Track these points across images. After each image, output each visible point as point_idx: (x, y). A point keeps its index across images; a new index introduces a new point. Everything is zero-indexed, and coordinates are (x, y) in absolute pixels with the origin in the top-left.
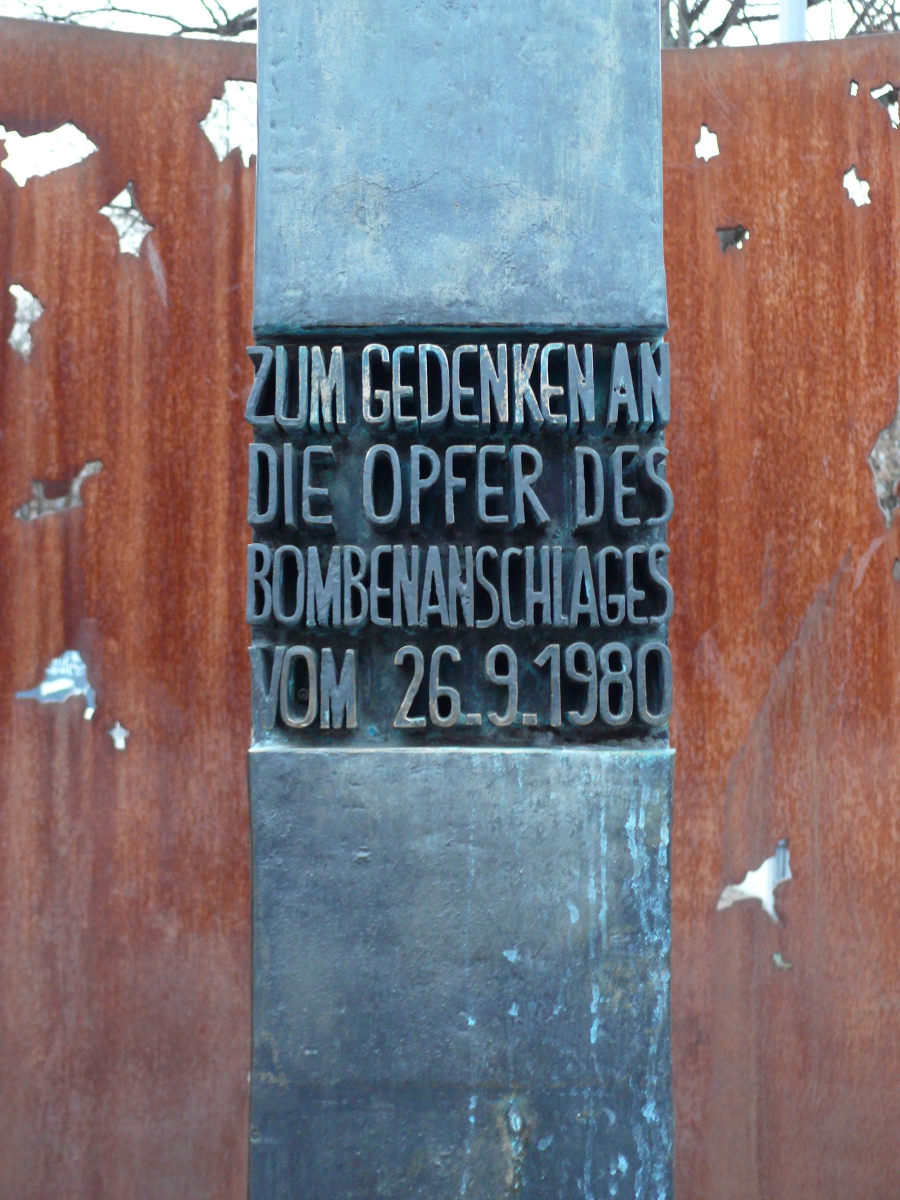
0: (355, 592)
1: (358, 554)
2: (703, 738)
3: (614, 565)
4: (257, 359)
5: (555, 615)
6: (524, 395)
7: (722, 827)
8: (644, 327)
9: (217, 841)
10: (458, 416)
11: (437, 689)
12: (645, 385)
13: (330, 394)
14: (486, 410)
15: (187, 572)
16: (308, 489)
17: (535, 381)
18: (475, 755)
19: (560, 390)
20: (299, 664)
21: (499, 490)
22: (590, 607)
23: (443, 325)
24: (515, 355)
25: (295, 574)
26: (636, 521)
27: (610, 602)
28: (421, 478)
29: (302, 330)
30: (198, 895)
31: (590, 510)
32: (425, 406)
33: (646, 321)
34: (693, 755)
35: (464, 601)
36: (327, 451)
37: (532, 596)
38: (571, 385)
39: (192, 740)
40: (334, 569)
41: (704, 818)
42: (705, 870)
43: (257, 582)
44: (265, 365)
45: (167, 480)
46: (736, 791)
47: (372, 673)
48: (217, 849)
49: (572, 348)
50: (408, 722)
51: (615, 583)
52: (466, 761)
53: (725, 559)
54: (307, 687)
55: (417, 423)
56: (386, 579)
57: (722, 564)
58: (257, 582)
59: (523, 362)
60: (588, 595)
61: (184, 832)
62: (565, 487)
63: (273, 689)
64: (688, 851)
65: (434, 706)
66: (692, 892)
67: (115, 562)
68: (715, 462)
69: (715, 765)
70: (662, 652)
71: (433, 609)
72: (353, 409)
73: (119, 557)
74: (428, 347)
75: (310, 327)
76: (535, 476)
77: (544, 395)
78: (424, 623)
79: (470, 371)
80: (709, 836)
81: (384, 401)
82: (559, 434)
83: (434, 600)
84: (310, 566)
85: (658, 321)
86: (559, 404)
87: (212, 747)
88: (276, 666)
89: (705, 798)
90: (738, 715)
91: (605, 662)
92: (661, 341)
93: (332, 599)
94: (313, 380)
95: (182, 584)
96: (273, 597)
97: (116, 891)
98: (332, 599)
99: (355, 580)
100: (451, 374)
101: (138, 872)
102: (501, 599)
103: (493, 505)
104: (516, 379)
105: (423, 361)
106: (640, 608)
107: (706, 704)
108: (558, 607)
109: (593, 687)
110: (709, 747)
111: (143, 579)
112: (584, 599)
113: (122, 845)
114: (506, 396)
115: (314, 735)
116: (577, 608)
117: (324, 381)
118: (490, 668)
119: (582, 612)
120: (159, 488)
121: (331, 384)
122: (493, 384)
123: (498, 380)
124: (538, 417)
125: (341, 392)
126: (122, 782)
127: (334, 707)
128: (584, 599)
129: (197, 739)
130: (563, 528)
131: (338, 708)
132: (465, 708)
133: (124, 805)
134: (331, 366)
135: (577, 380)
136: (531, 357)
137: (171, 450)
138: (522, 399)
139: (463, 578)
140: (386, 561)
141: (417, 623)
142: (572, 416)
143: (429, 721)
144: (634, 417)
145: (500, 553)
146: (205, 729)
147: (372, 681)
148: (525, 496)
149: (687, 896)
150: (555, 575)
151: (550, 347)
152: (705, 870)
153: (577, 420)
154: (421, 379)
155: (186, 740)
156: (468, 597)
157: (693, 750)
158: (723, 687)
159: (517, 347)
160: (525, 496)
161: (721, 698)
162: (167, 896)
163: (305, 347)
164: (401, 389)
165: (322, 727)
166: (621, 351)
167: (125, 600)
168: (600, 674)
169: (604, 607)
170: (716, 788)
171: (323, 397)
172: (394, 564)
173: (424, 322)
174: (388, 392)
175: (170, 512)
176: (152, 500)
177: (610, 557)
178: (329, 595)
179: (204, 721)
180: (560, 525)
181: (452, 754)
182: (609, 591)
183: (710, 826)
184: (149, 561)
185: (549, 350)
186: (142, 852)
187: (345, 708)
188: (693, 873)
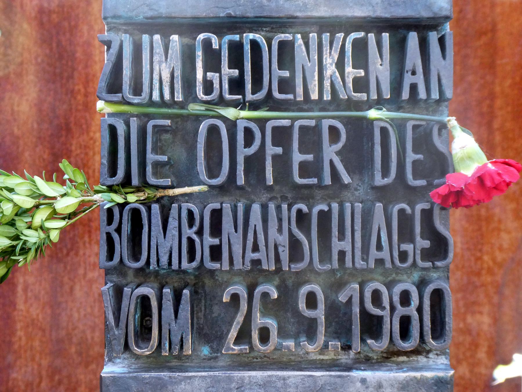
0: (191, 241)
1: (192, 209)
2: (480, 250)
3: (405, 221)
4: (109, 44)
5: (356, 260)
6: (331, 76)
7: (496, 320)
8: (433, 18)
9: (97, 334)
10: (276, 95)
11: (259, 320)
12: (432, 68)
13: (169, 76)
14: (300, 90)
15: (72, 119)
16: (151, 157)
17: (340, 65)
18: (289, 377)
19: (362, 73)
20: (145, 300)
21: (310, 157)
22: (385, 254)
23: (264, 17)
24: (324, 42)
25: (141, 227)
26: (421, 183)
27: (401, 250)
28: (245, 148)
29: (146, 20)
30: (82, 377)
31: (385, 173)
32: (249, 86)
33: (434, 13)
34: (473, 264)
35: (280, 249)
36: (167, 124)
37: (337, 245)
38: (371, 68)
39: (77, 254)
40: (173, 223)
41: (481, 313)
42: (482, 354)
43: (109, 235)
44: (114, 50)
45: (54, 45)
46: (507, 292)
47: (206, 302)
48: (97, 339)
49: (372, 36)
50: (234, 350)
51: (406, 233)
52: (282, 382)
53: (501, 109)
54: (151, 316)
55: (242, 101)
56: (216, 229)
57: (499, 113)
58: (109, 235)
59: (331, 48)
60: (383, 244)
61: (70, 327)
62: (365, 147)
63: (122, 324)
64: (468, 339)
65: (255, 336)
66: (471, 372)
67: (13, 112)
68: (494, 30)
69: (490, 271)
70: (444, 291)
71: (256, 256)
72: (189, 84)
73: (16, 108)
74: (251, 36)
75: (151, 18)
76: (340, 145)
77: (348, 77)
78: (248, 266)
79: (286, 51)
80: (485, 328)
81: (214, 81)
82: (360, 104)
83: (256, 248)
84: (153, 221)
85: (444, 13)
86: (361, 85)
87: (92, 259)
88: (125, 302)
89: (482, 297)
90: (509, 232)
91: (396, 299)
92: (447, 28)
93: (171, 248)
94: (154, 64)
95: (68, 130)
96: (122, 247)
97: (14, 375)
98: (171, 248)
99: (189, 232)
100: (270, 59)
101: (33, 360)
102: (310, 245)
103: (305, 169)
104: (324, 63)
105: (247, 48)
106: (427, 255)
107: (484, 223)
108: (358, 253)
109: (387, 320)
110: (486, 258)
111: (35, 126)
112: (379, 247)
113: (20, 339)
114: (316, 78)
115: (157, 362)
116: (374, 253)
117: (164, 65)
118: (302, 305)
119: (378, 257)
120: (48, 51)
121: (169, 68)
122: (306, 68)
123: (309, 65)
124: (343, 96)
125: (178, 73)
126: (20, 289)
127: (173, 338)
128: (379, 247)
129: (81, 252)
130: (363, 182)
131: (176, 340)
132: (282, 333)
133: (21, 306)
134: (170, 51)
135: (375, 64)
136: (337, 45)
137: (56, 20)
138: (329, 80)
139: (280, 230)
140: (217, 215)
141: (241, 267)
142: (371, 94)
143: (252, 348)
144: (422, 94)
145: (310, 209)
146: (87, 245)
147: (205, 309)
148: (331, 162)
149: (468, 375)
150: (356, 228)
151: (354, 35)
152: (482, 354)
153: (376, 97)
154: (246, 63)
155: (72, 253)
156: (284, 246)
157: (473, 259)
158: (497, 210)
159: (326, 36)
160: (331, 162)
161: (496, 219)
162: (57, 378)
163: (147, 36)
164: (228, 72)
165: (164, 354)
166: (413, 38)
167: (21, 142)
168: (393, 309)
169: (396, 254)
170: (491, 290)
171: (163, 78)
172: (223, 218)
173: (249, 15)
174: (218, 75)
175: (58, 71)
176: (43, 61)
177: (402, 212)
178: (169, 245)
179: (86, 239)
180: (361, 180)
181: (269, 376)
182: (402, 239)
183: (486, 320)
184: (40, 111)
185: (353, 38)
186: (36, 344)
187: (182, 338)
188: (472, 356)
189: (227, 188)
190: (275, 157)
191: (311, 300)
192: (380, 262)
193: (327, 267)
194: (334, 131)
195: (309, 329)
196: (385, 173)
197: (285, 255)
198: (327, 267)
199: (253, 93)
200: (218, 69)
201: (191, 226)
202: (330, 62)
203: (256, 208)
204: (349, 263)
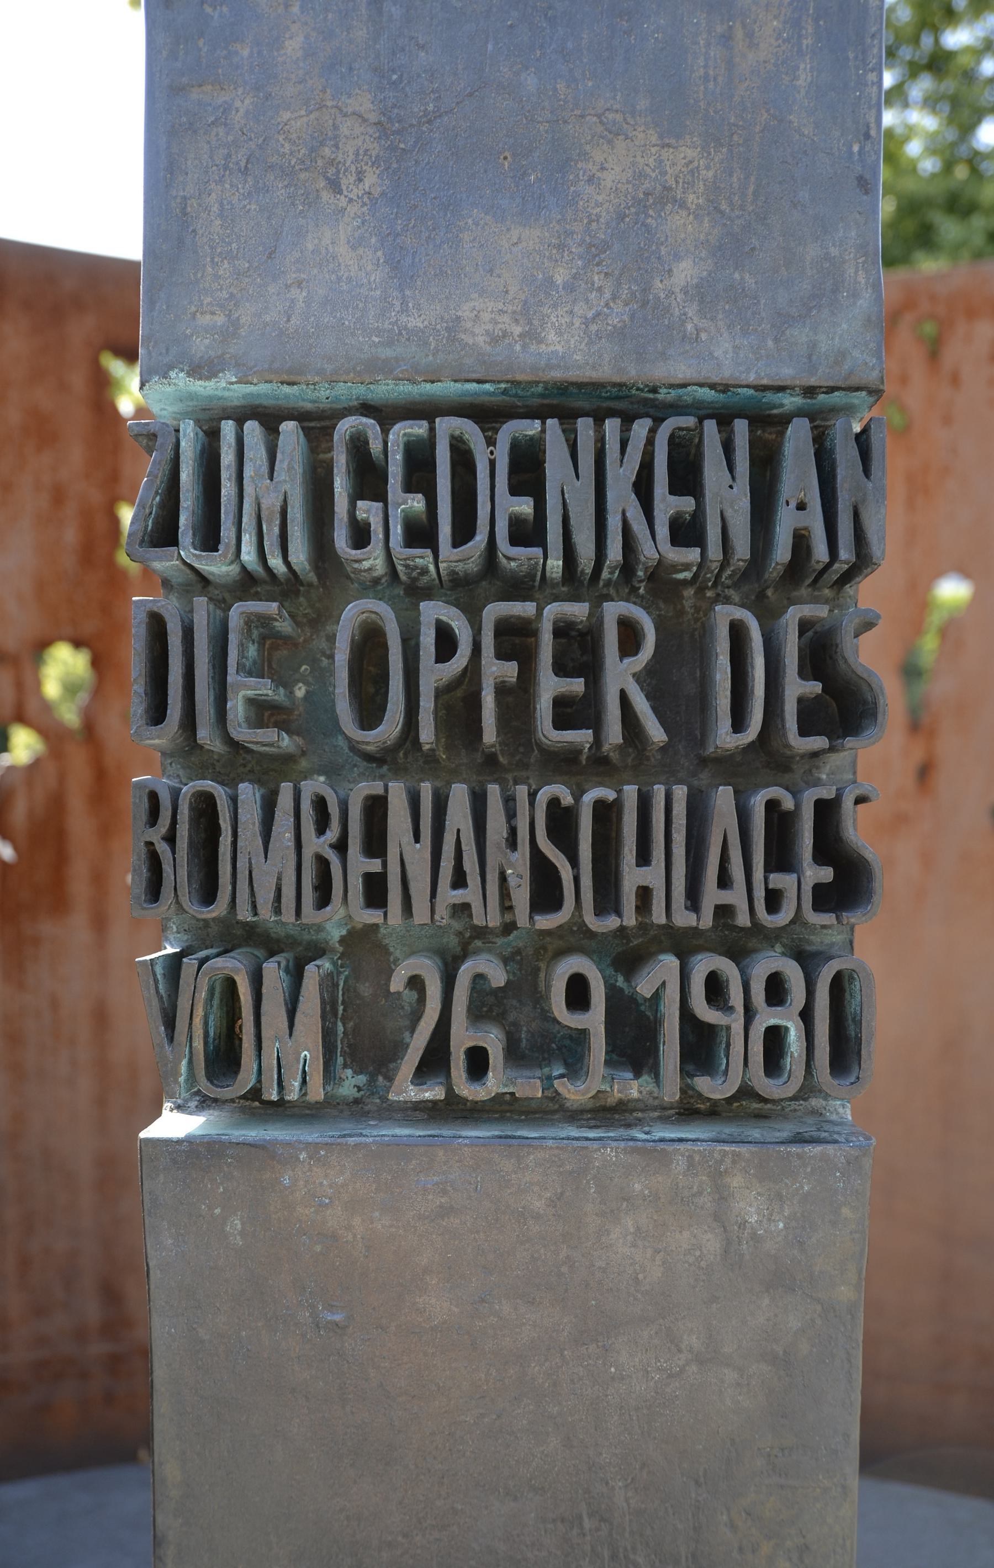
0: (323, 864)
3: (780, 823)
27: (771, 886)
31: (738, 724)
37: (632, 877)
51: (781, 856)
56: (376, 843)
71: (458, 896)
83: (459, 881)
99: (315, 844)
103: (567, 713)
106: (824, 898)
112: (724, 881)
116: (712, 896)
128: (724, 881)
132: (514, 1054)
140: (376, 809)
145: (577, 797)
159: (612, 426)
169: (759, 894)
174: (380, 505)
189: (401, 755)
190: (502, 690)
191: (578, 993)
192: (724, 911)
193: (612, 922)
194: (630, 639)
195: (571, 1050)
196: (738, 724)
197: (521, 896)
198: (612, 922)
199: (456, 544)
200: (380, 495)
201: (321, 831)
202: (621, 478)
203: (459, 795)
204: (658, 916)
